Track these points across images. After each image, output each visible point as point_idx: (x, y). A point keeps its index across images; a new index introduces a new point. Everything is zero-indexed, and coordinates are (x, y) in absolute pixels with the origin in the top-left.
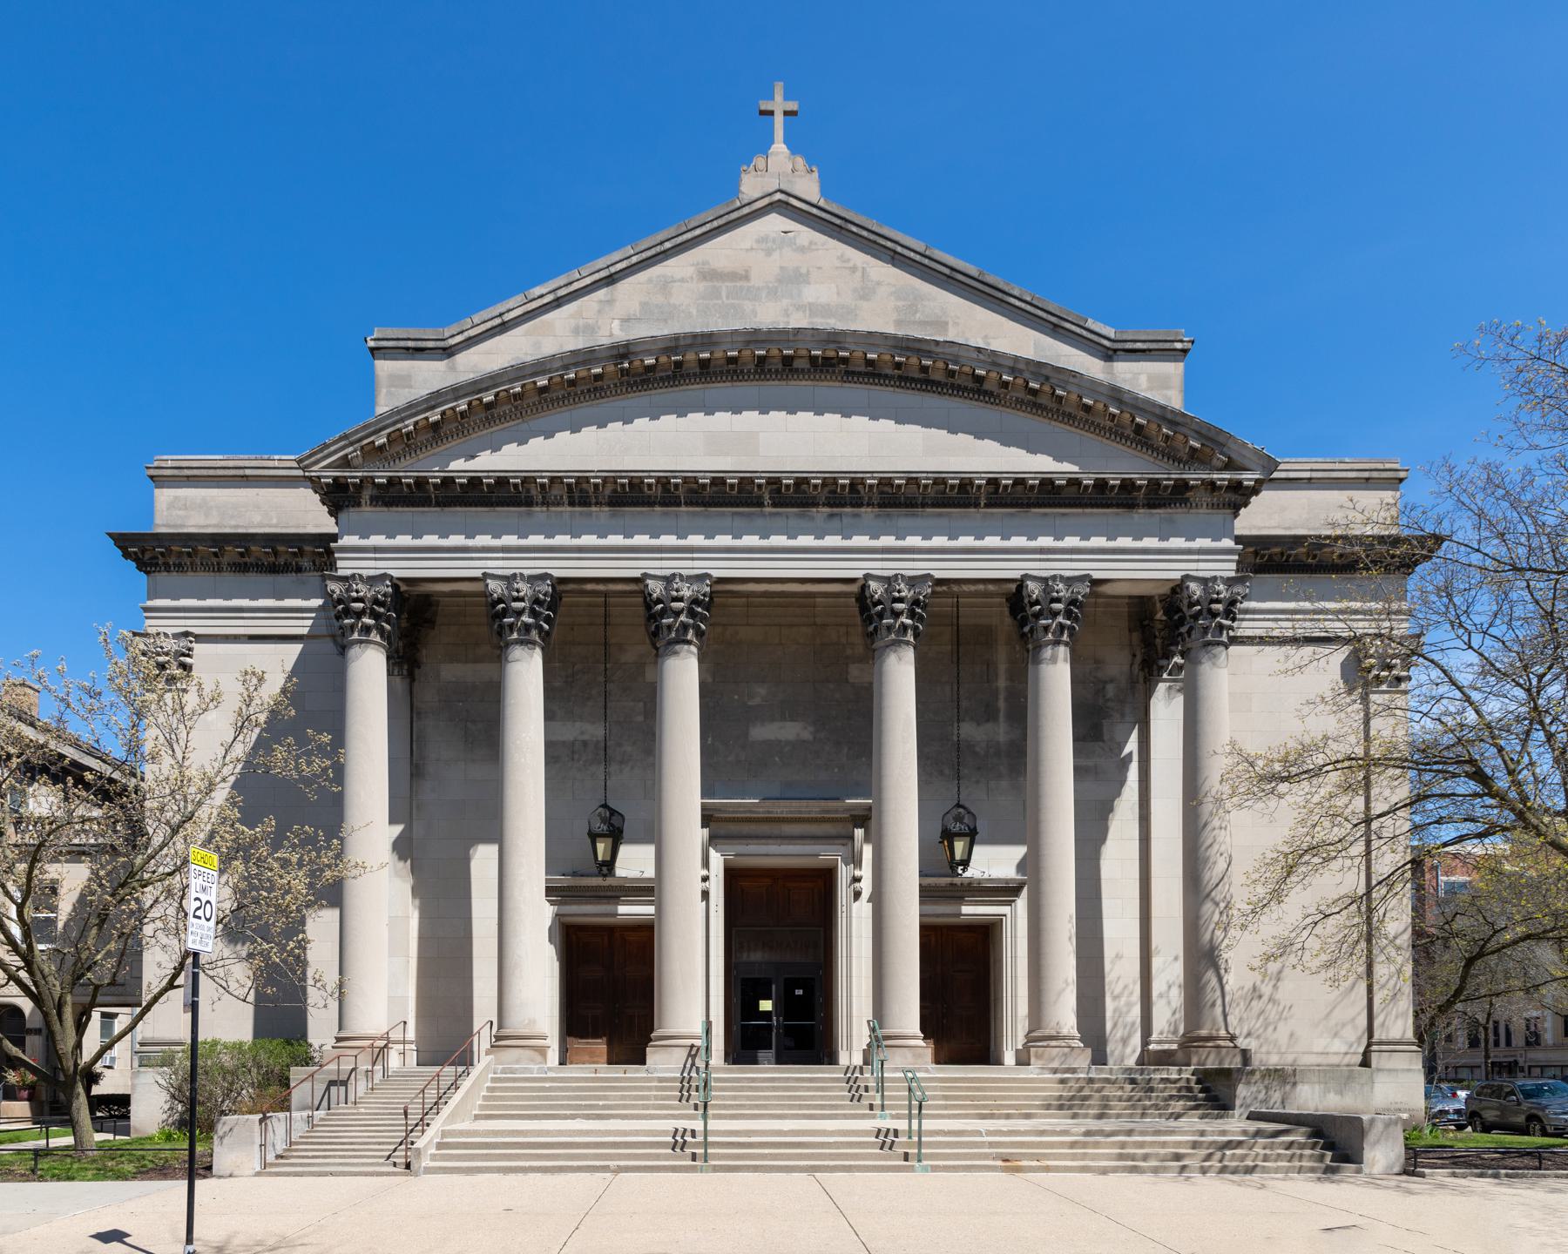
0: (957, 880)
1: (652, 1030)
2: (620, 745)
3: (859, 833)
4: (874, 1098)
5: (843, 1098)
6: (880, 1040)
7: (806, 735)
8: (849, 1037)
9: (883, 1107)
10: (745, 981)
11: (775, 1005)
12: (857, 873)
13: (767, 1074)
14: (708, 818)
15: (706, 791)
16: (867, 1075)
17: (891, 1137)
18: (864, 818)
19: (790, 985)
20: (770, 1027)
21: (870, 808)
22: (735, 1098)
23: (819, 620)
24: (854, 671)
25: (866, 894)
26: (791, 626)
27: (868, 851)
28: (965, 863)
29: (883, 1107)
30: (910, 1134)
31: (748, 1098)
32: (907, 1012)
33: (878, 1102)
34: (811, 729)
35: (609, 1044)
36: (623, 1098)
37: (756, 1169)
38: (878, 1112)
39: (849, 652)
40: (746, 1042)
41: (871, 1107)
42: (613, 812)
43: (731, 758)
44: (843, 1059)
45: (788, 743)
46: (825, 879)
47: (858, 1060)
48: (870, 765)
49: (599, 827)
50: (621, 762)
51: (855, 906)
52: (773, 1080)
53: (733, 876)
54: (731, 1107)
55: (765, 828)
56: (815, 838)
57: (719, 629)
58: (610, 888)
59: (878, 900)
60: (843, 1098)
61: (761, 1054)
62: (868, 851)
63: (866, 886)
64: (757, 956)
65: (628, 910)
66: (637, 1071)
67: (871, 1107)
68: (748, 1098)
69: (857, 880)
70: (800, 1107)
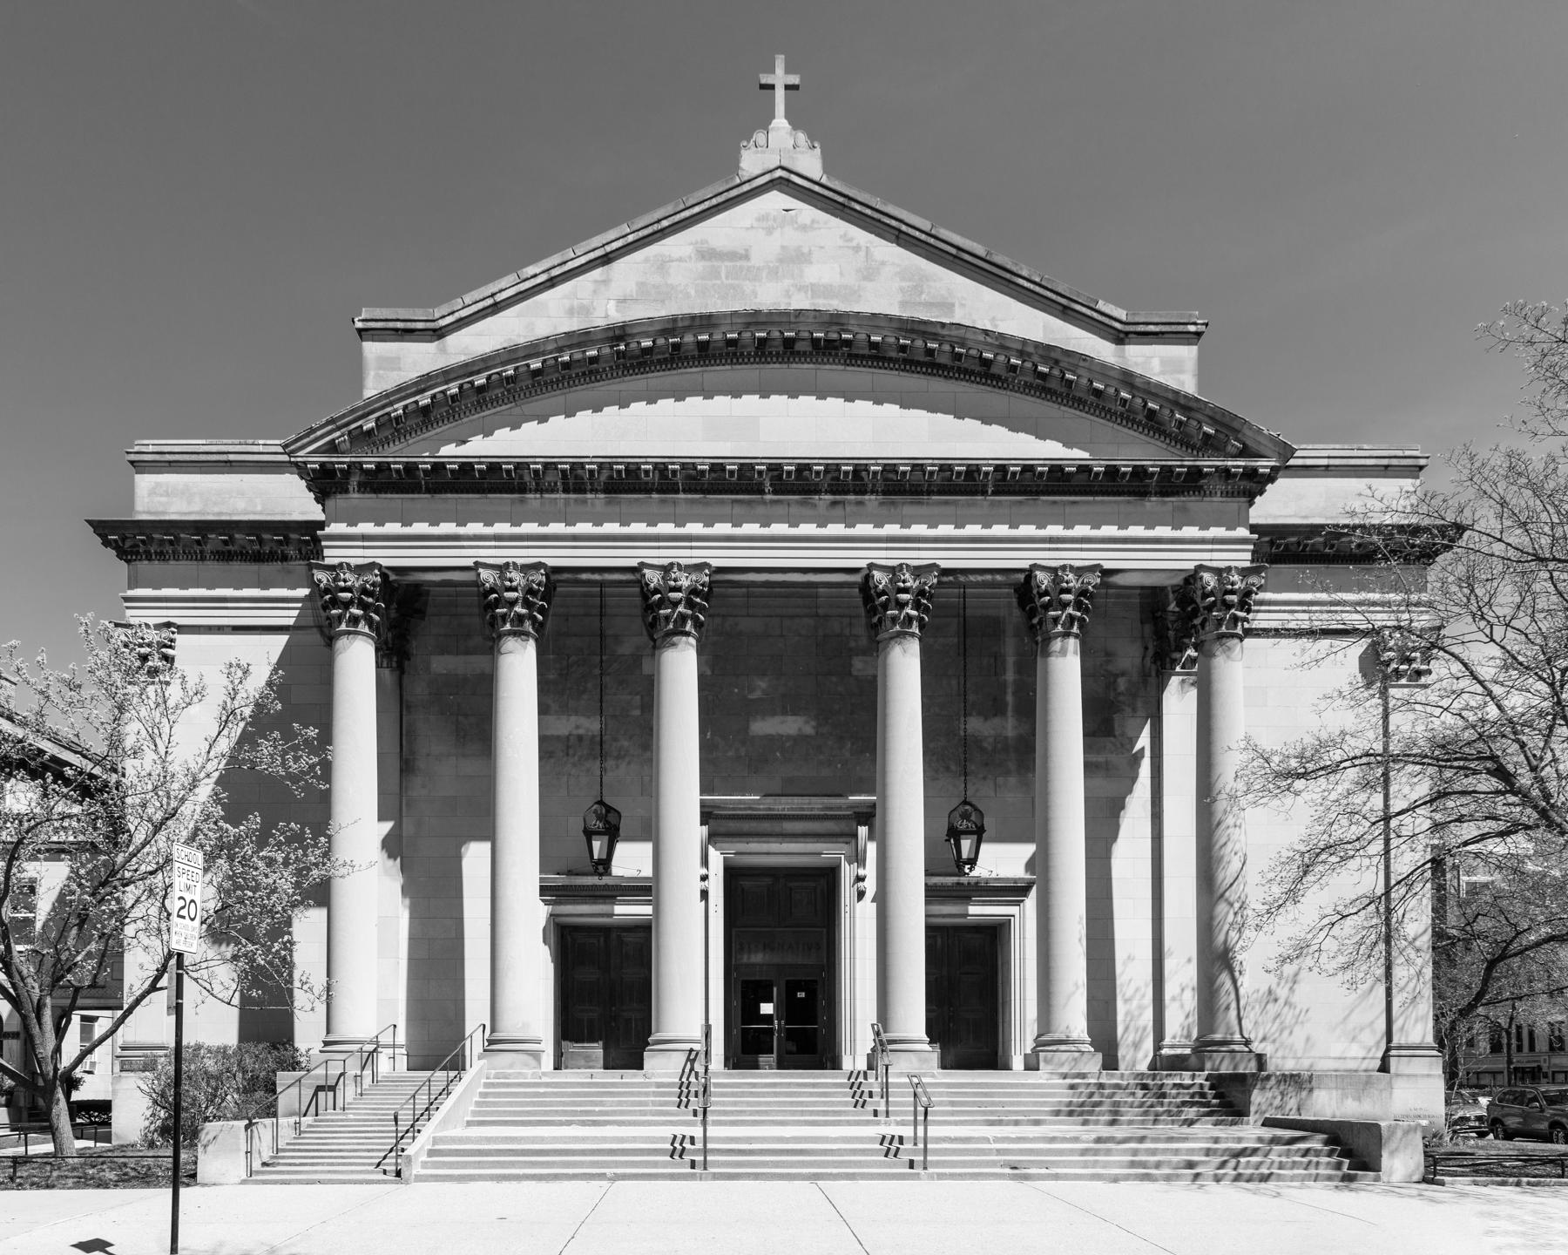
0: (964, 880)
1: (650, 1034)
2: (616, 740)
3: (863, 831)
5: (846, 1104)
6: (884, 1044)
7: (809, 730)
8: (853, 1041)
10: (746, 984)
11: (776, 1008)
12: (861, 872)
13: (768, 1079)
14: (707, 816)
16: (871, 1080)
18: (868, 816)
19: (792, 987)
20: (771, 1031)
21: (873, 805)
22: (735, 1104)
23: (821, 611)
24: (858, 664)
25: (870, 894)
26: (792, 617)
27: (872, 849)
28: (972, 862)
31: (749, 1104)
33: (882, 1108)
34: (813, 723)
35: (605, 1049)
36: (620, 1103)
39: (853, 644)
40: (746, 1047)
42: (609, 809)
43: (730, 754)
44: (847, 1063)
45: (789, 737)
47: (862, 1065)
48: (874, 761)
50: (618, 758)
51: (859, 906)
53: (732, 874)
54: (732, 1113)
55: (766, 826)
57: (718, 620)
58: (606, 887)
59: (882, 899)
60: (846, 1104)
61: (763, 1059)
62: (872, 849)
63: (870, 886)
64: (758, 958)
65: (625, 910)
66: (635, 1076)
68: (749, 1104)
70: (802, 1113)
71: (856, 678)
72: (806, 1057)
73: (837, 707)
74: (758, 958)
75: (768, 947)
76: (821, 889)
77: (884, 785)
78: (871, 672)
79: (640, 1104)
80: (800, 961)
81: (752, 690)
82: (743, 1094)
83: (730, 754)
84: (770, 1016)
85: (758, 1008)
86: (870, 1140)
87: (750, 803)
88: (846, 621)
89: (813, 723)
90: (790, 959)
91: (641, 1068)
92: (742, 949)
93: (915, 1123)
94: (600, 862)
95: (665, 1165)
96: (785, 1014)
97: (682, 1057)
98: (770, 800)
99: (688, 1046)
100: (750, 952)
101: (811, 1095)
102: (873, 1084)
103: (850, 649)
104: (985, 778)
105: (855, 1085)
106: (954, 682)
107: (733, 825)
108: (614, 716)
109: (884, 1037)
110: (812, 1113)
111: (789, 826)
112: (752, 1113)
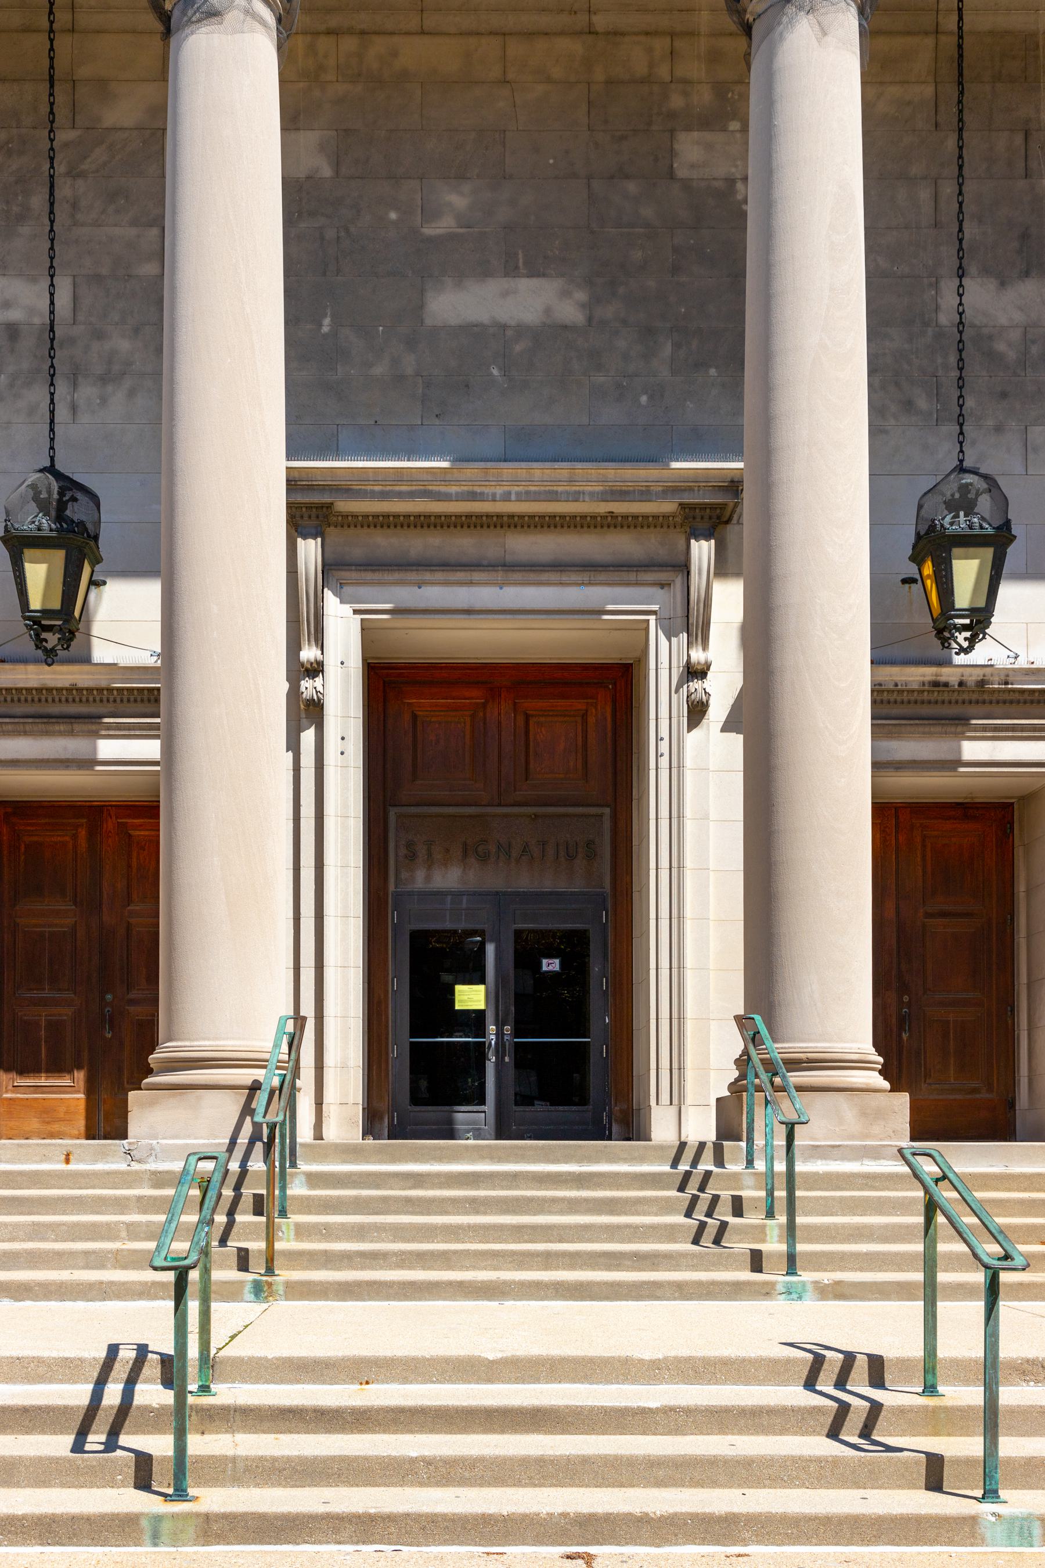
0: (946, 674)
1: (152, 1044)
2: (99, 335)
3: (702, 551)
4: (760, 1233)
5: (670, 1233)
6: (765, 1073)
7: (570, 311)
8: (677, 1069)
9: (792, 1262)
10: (419, 940)
11: (494, 997)
12: (698, 655)
13: (473, 1163)
14: (309, 511)
15: (309, 424)
16: (735, 1167)
17: (859, 1384)
18: (715, 514)
19: (526, 953)
20: (480, 1050)
21: (734, 486)
22: (360, 1232)
23: (600, 22)
24: (691, 150)
25: (718, 711)
26: (530, 35)
27: (728, 602)
28: (980, 621)
29: (792, 1262)
30: (930, 1372)
31: (399, 1232)
32: (839, 1001)
33: (774, 1245)
34: (581, 296)
35: (91, 1090)
36: (37, 1232)
37: (366, 1528)
38: (781, 1279)
39: (677, 102)
40: (423, 1080)
41: (757, 1261)
42: (69, 486)
43: (379, 370)
44: (662, 1127)
45: (522, 330)
46: (611, 690)
47: (701, 1127)
48: (735, 388)
49: (34, 521)
50: (104, 379)
51: (693, 739)
52: (513, 1180)
53: (390, 682)
54: (346, 1259)
55: (464, 544)
56: (591, 569)
57: (349, 44)
58: (74, 693)
59: (758, 717)
60: (670, 1233)
61: (463, 1115)
62: (728, 602)
63: (723, 687)
64: (449, 878)
65: (124, 750)
66: (102, 1156)
67: (757, 1261)
68: (399, 1232)
69: (695, 672)
70: (548, 1260)
71: (686, 185)
72: (562, 1111)
73: (637, 255)
74: (449, 878)
75: (474, 851)
76: (595, 711)
77: (767, 422)
78: (721, 169)
79: (94, 1232)
81: (430, 214)
82: (385, 1206)
83: (379, 370)
84: (479, 1016)
86: (768, 1370)
87: (422, 486)
88: (661, 45)
89: (581, 296)
90: (525, 881)
91: (121, 1133)
92: (412, 856)
93: (991, 1371)
94: (38, 624)
95: (42, 1473)
96: (508, 1008)
97: (230, 1106)
98: (472, 470)
99: (246, 1076)
100: (430, 863)
101: (573, 1206)
102: (740, 1175)
103: (672, 115)
104: (999, 429)
105: (691, 1176)
106: (925, 194)
107: (385, 542)
108: (97, 279)
109: (777, 1050)
110: (574, 1260)
112: (405, 1260)
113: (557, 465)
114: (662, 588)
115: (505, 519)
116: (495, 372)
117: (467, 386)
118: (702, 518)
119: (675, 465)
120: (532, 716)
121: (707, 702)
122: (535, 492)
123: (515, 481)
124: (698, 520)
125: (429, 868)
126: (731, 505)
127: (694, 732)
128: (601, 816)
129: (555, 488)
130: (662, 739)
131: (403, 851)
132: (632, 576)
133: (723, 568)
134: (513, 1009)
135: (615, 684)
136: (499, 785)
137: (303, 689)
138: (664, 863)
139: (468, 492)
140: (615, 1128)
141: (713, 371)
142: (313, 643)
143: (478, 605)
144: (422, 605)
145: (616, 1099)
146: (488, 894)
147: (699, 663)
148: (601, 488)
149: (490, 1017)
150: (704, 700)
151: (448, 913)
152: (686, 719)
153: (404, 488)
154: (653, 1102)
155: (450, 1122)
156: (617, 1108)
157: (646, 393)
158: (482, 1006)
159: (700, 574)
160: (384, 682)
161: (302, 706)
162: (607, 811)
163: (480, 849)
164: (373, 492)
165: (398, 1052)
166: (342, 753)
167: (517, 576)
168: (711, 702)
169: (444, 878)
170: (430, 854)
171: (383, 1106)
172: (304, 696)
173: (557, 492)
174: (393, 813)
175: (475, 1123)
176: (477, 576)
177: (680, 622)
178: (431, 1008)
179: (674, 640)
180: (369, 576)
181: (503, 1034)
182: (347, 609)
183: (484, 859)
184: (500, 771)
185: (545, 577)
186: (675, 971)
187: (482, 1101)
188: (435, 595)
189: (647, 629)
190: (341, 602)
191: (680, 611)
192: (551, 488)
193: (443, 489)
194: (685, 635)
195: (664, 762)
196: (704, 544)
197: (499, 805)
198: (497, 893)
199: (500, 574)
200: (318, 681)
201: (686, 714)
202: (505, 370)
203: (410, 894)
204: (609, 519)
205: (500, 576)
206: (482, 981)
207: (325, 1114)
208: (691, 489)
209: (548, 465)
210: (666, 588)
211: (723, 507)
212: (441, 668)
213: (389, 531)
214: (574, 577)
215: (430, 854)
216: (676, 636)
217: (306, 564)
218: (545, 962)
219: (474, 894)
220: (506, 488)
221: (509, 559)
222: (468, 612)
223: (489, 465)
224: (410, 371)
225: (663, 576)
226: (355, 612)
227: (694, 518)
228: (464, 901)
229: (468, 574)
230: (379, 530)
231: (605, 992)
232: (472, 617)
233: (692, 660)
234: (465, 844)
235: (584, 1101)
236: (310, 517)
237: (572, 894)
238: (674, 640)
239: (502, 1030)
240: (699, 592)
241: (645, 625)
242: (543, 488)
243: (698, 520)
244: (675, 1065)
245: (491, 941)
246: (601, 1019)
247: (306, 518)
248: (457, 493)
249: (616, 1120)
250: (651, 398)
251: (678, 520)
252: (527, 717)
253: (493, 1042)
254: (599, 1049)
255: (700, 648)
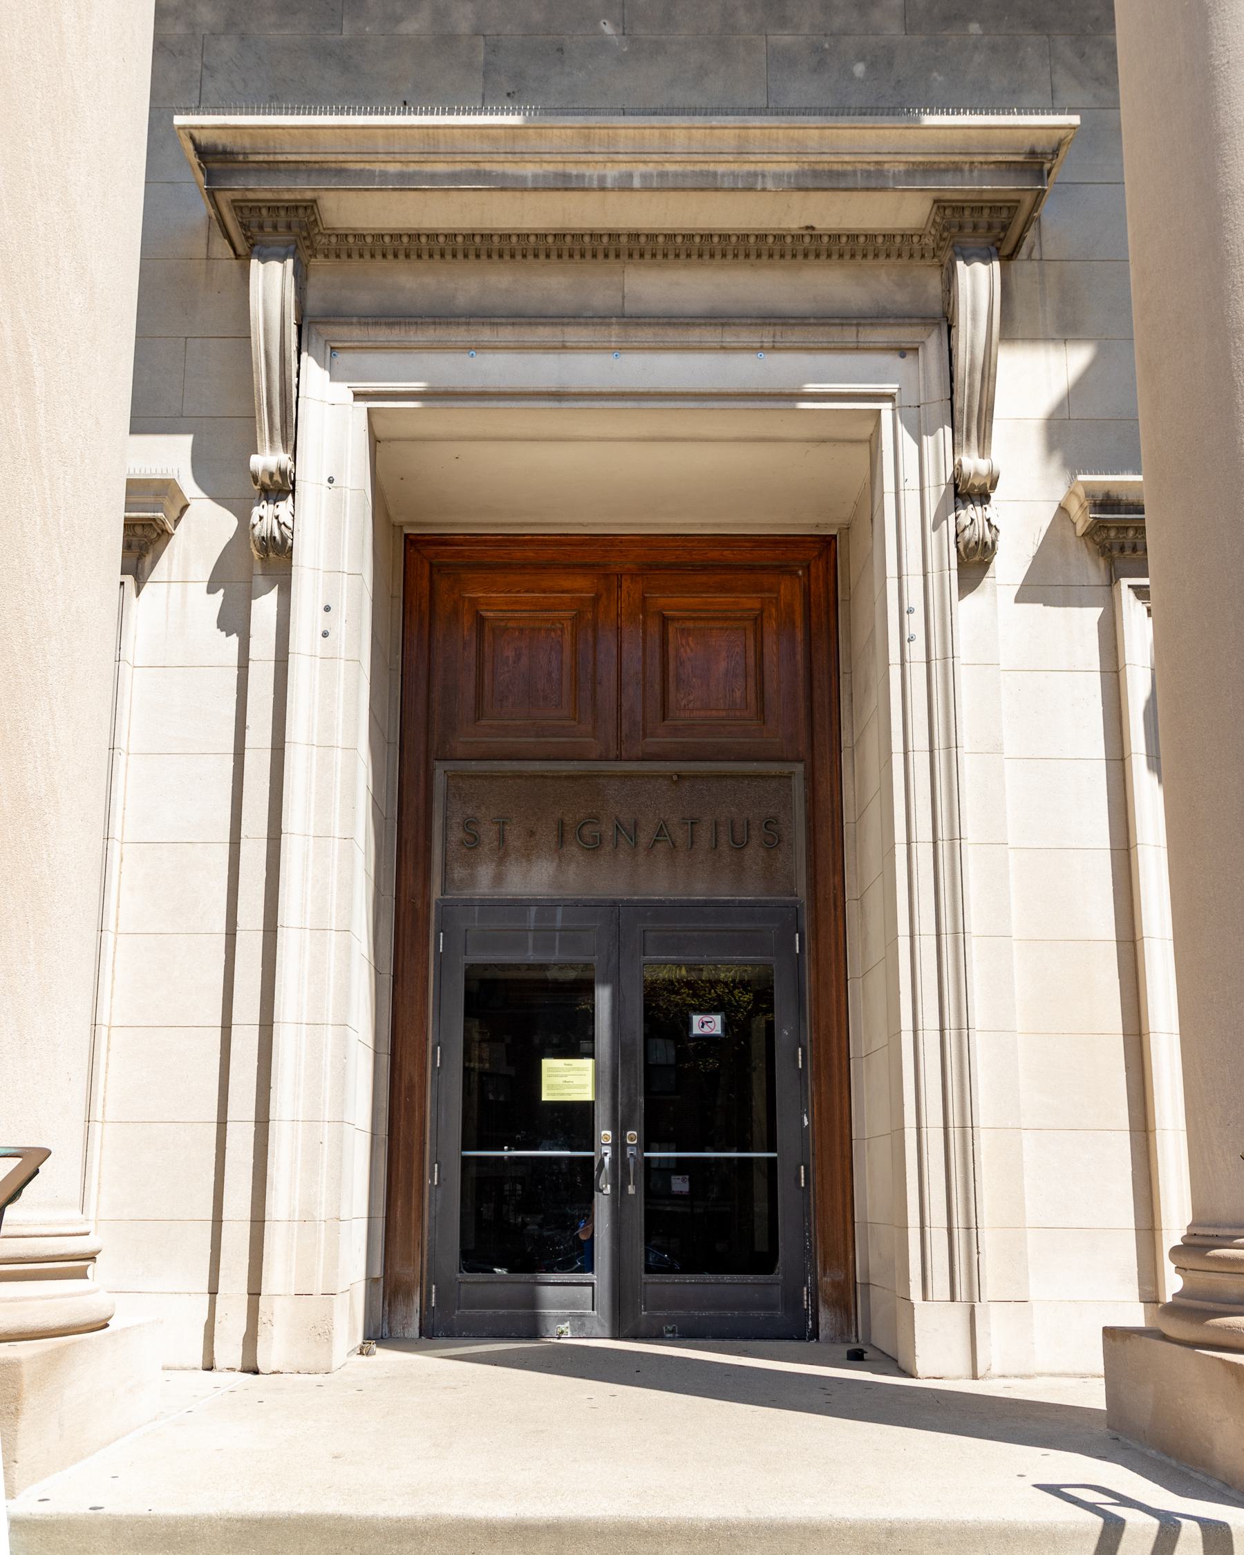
3: (977, 282)
11: (611, 1080)
12: (972, 463)
19: (661, 1015)
21: (1035, 163)
25: (1010, 566)
43: (410, 27)
51: (969, 609)
55: (552, 284)
64: (534, 878)
69: (968, 492)
72: (488, 975)
74: (534, 878)
75: (576, 835)
80: (700, 890)
85: (534, 1079)
90: (661, 883)
92: (473, 842)
100: (502, 852)
111: (651, 285)
113: (715, 121)
114: (903, 356)
115: (624, 239)
116: (608, 29)
117: (560, 50)
118: (975, 227)
119: (929, 120)
120: (673, 619)
121: (993, 543)
122: (676, 175)
123: (639, 153)
124: (968, 230)
125: (501, 861)
126: (1028, 200)
127: (970, 598)
128: (789, 777)
129: (712, 167)
130: (910, 611)
131: (457, 835)
132: (849, 335)
133: (1012, 325)
134: (642, 1100)
135: (807, 569)
136: (619, 726)
137: (255, 519)
138: (923, 831)
139: (556, 175)
140: (824, 1316)
141: (974, 28)
142: (279, 444)
143: (575, 385)
144: (476, 384)
145: (825, 1270)
146: (598, 904)
147: (977, 474)
148: (793, 167)
149: (602, 1115)
150: (989, 539)
151: (530, 935)
152: (954, 574)
153: (441, 168)
154: (915, 1294)
155: (532, 1302)
156: (827, 1279)
157: (863, 59)
158: (587, 1095)
159: (974, 319)
160: (431, 565)
161: (255, 553)
162: (799, 768)
163: (586, 831)
164: (384, 175)
165: (442, 1178)
166: (325, 635)
167: (645, 335)
168: (999, 544)
169: (526, 882)
170: (502, 839)
171: (411, 1272)
172: (257, 531)
173: (715, 174)
174: (440, 771)
175: (573, 1305)
176: (573, 334)
177: (938, 408)
178: (500, 1101)
179: (928, 441)
180: (382, 334)
181: (625, 1145)
182: (343, 391)
183: (593, 847)
184: (619, 706)
185: (694, 335)
186: (951, 1036)
187: (589, 1267)
188: (498, 367)
189: (873, 442)
190: (332, 380)
191: (937, 390)
192: (705, 167)
193: (510, 169)
194: (948, 430)
195: (916, 651)
196: (980, 268)
197: (618, 758)
198: (614, 904)
199: (615, 330)
200: (284, 508)
201: (954, 565)
202: (624, 27)
203: (469, 903)
204: (807, 239)
205: (614, 334)
206: (591, 1055)
207: (262, 1317)
208: (956, 168)
209: (699, 120)
210: (910, 357)
211: (1012, 207)
212: (526, 542)
213: (419, 265)
214: (747, 336)
215: (502, 839)
216: (932, 433)
217: (265, 302)
218: (696, 1019)
219: (576, 903)
220: (624, 168)
221: (630, 308)
222: (557, 396)
223: (593, 121)
224: (464, 27)
225: (904, 335)
226: (358, 396)
227: (961, 228)
228: (559, 917)
229: (557, 330)
230: (401, 263)
231: (802, 1073)
232: (565, 405)
233: (965, 469)
234: (562, 824)
235: (765, 1263)
236: (275, 227)
237: (742, 904)
238: (928, 441)
239: (623, 1137)
240: (972, 347)
241: (868, 429)
242: (690, 168)
243: (968, 230)
244: (959, 1221)
245: (604, 982)
246: (797, 1121)
247: (268, 230)
248: (535, 177)
249: (825, 1302)
250: (872, 67)
251: (929, 241)
252: (665, 621)
253: (607, 1160)
254: (794, 1177)
255: (975, 454)
